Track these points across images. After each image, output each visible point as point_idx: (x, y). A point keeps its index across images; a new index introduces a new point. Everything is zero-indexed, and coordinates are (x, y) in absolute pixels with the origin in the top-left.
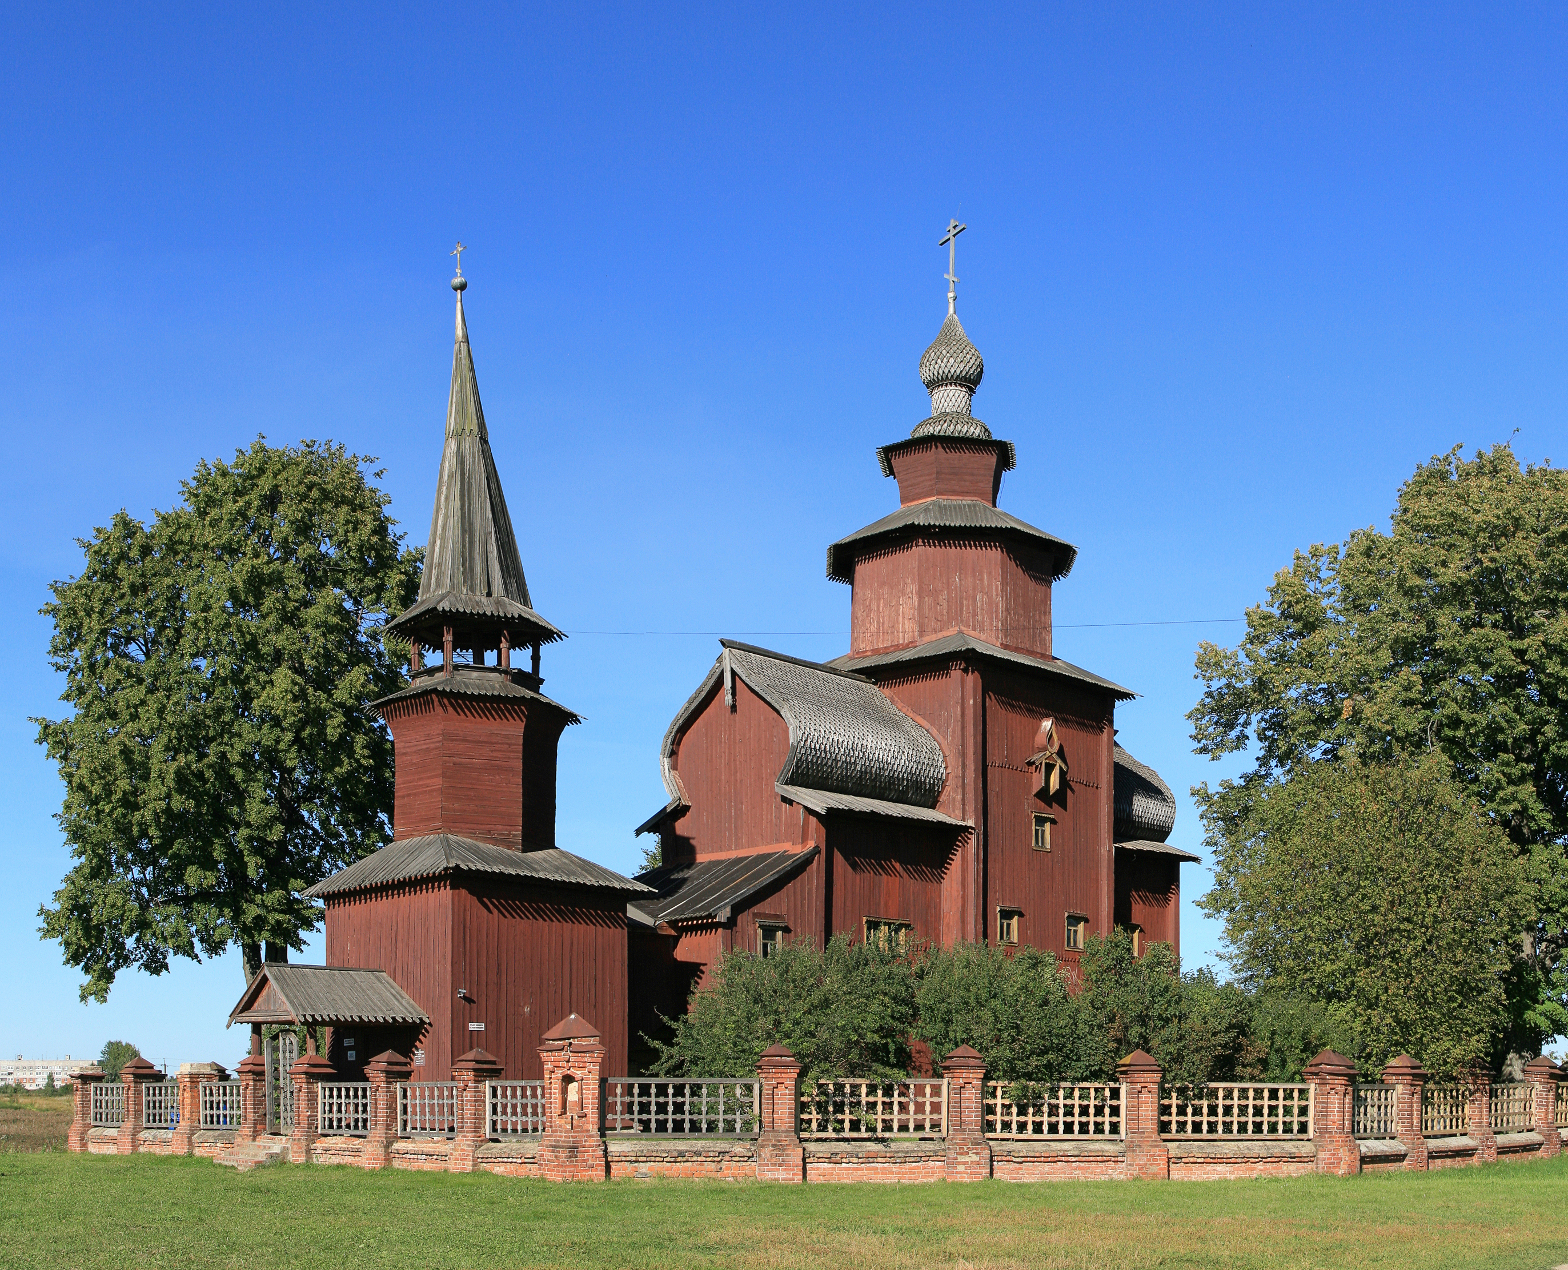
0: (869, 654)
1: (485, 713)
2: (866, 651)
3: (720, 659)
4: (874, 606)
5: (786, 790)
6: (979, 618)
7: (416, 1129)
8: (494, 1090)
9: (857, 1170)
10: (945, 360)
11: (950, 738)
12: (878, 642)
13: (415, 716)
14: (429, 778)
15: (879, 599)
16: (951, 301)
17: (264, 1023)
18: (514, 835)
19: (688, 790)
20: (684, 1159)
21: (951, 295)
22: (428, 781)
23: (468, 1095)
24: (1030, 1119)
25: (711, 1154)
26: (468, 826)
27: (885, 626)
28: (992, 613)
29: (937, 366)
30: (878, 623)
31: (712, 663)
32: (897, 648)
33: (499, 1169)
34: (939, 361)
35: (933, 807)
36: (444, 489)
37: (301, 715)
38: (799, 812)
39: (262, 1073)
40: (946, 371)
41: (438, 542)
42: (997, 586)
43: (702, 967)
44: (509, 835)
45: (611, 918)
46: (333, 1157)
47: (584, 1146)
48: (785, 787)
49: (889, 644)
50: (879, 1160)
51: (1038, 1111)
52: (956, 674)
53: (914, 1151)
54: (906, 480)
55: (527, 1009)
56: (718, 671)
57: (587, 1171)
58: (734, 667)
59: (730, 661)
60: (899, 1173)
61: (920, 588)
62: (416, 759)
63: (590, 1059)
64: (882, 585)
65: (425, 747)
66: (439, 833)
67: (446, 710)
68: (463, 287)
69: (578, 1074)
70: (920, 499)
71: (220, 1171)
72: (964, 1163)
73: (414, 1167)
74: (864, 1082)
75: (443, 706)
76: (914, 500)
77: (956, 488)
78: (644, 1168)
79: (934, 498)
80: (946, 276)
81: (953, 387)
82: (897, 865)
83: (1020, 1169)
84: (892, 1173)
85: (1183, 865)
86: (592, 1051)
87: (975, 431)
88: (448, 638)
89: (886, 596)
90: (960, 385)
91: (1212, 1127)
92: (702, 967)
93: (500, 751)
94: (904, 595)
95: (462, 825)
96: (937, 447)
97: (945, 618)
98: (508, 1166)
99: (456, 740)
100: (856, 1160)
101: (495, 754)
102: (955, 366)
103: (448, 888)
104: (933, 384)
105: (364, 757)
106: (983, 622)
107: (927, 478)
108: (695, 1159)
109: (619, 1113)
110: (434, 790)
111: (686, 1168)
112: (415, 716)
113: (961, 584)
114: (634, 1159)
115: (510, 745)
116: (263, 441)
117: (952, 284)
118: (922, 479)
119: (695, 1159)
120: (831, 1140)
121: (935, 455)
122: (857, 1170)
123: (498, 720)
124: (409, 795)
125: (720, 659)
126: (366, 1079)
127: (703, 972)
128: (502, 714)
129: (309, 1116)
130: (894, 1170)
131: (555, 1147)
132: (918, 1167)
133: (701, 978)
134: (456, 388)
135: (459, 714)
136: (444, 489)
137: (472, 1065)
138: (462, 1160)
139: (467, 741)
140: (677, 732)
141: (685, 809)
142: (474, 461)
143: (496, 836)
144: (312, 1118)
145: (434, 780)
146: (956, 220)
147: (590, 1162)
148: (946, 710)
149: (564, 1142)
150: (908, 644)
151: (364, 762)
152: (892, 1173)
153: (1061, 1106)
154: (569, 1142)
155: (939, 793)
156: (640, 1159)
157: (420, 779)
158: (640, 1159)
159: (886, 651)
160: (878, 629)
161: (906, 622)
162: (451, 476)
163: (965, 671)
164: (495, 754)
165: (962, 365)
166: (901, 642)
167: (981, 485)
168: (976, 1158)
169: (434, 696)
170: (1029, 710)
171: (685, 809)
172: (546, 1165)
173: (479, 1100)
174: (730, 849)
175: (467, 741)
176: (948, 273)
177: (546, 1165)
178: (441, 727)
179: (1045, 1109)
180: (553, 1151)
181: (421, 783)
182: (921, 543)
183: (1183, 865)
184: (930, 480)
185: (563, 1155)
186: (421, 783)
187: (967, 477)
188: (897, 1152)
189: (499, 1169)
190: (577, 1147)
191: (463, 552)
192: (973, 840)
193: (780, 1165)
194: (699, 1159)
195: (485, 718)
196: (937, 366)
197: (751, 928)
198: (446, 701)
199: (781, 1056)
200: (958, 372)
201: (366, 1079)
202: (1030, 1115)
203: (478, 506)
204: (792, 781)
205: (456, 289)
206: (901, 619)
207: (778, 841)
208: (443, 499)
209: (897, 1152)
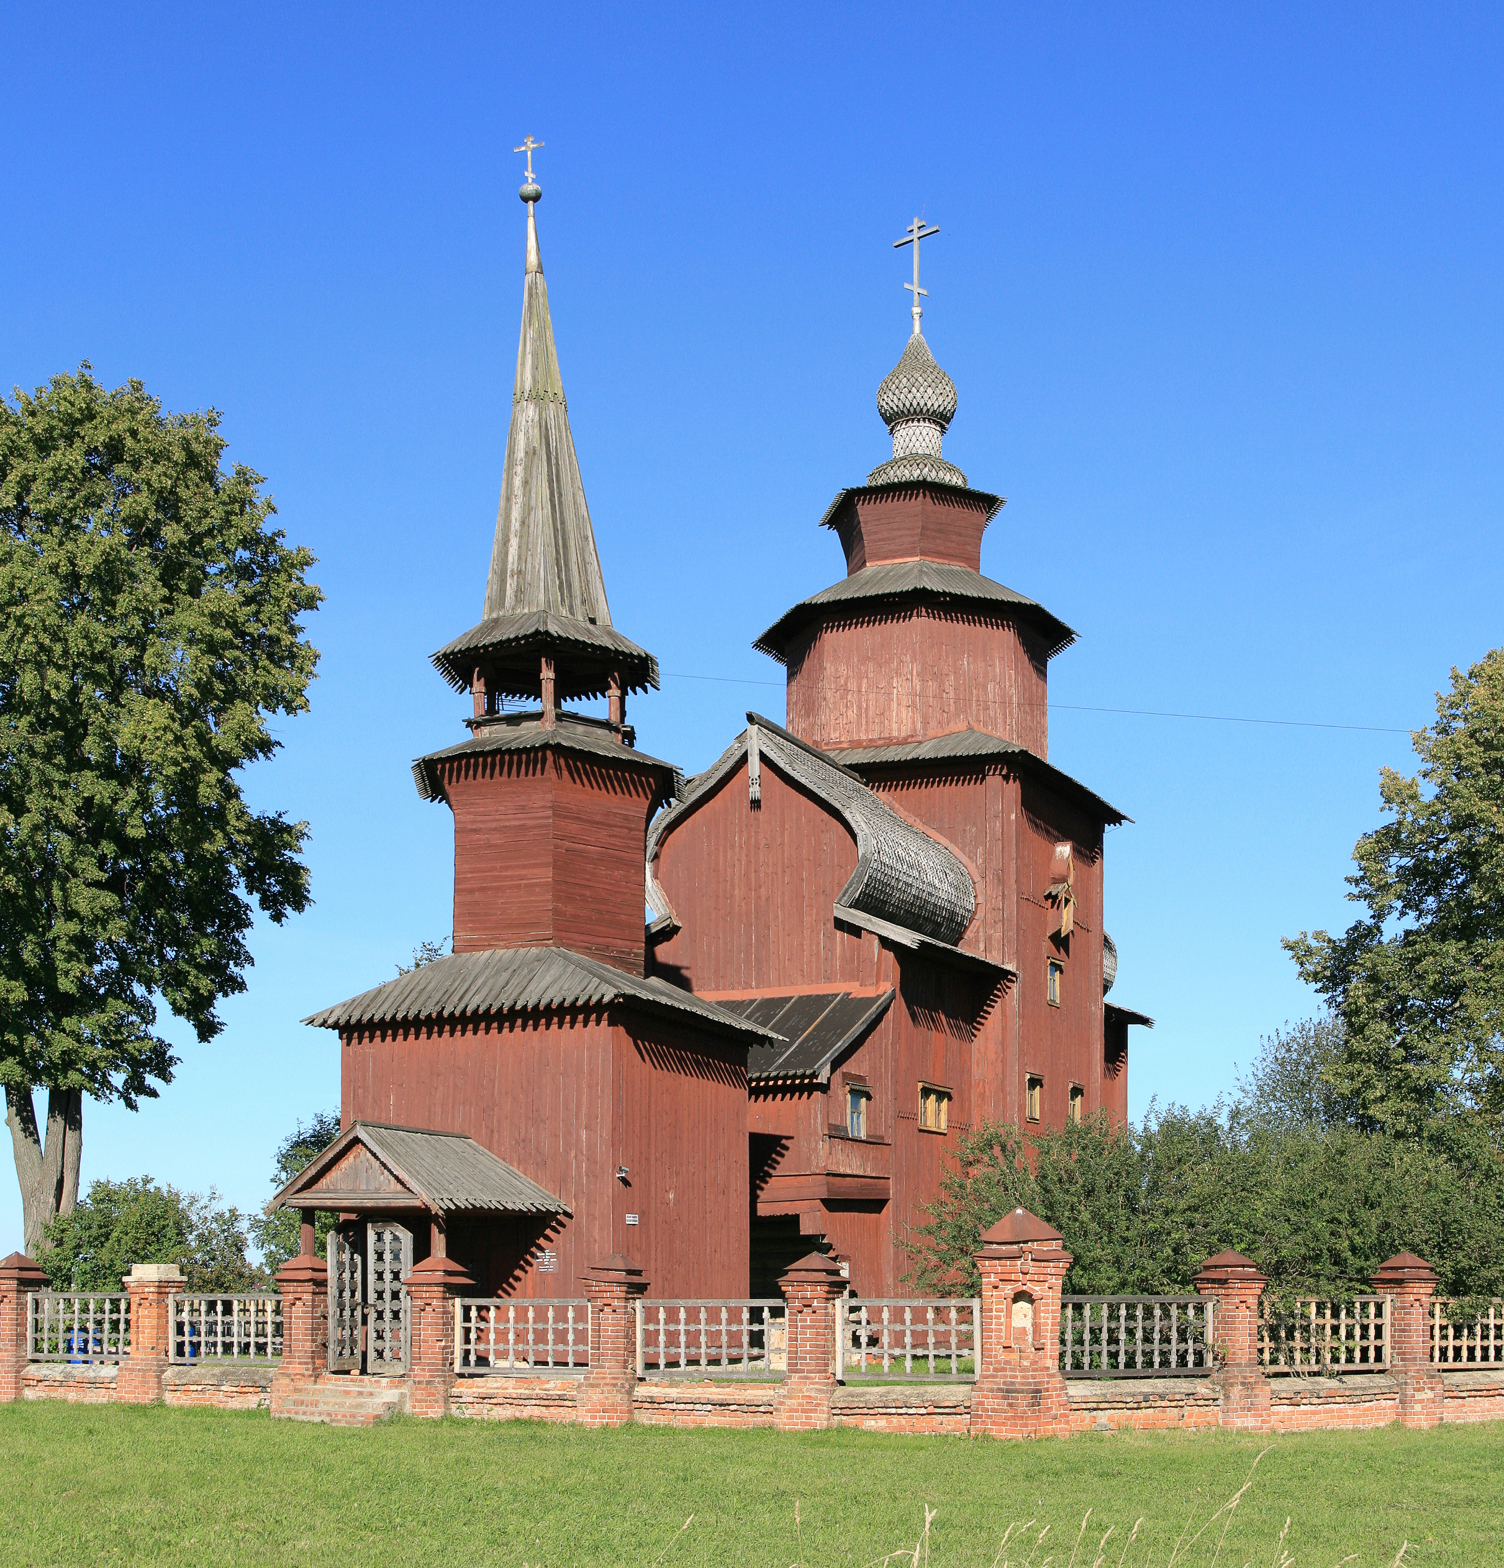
0: (845, 745)
1: (606, 783)
2: (841, 742)
3: (741, 737)
4: (852, 685)
5: (852, 914)
6: (992, 714)
7: (655, 1366)
8: (467, 1309)
9: (1314, 1413)
10: (922, 389)
11: (980, 861)
12: (859, 731)
13: (504, 778)
14: (524, 867)
15: (860, 678)
16: (916, 317)
17: (321, 1208)
18: (636, 955)
19: (677, 906)
20: (1148, 1404)
21: (916, 310)
22: (524, 872)
23: (429, 1316)
24: (1464, 1342)
25: (1178, 1397)
26: (582, 937)
27: (871, 713)
28: (1005, 708)
29: (910, 396)
30: (859, 707)
31: (730, 742)
32: (889, 742)
33: (870, 1424)
34: (914, 390)
35: (922, 942)
36: (519, 469)
37: (186, 765)
38: (871, 945)
39: (323, 1283)
40: (922, 404)
41: (514, 542)
42: (1010, 675)
43: (784, 1142)
44: (629, 954)
45: (736, 1073)
46: (496, 1408)
47: (1047, 1390)
48: (852, 910)
49: (876, 736)
50: (1338, 1399)
51: (1472, 1334)
52: (994, 781)
53: (1371, 1388)
54: (876, 533)
55: (671, 1196)
56: (738, 754)
57: (1050, 1423)
58: (765, 750)
59: (757, 741)
60: (1353, 1416)
61: (924, 668)
62: (497, 839)
63: (1053, 1271)
64: (864, 660)
65: (517, 823)
66: (547, 946)
67: (560, 776)
68: (536, 198)
69: (1036, 1290)
70: (895, 557)
71: (683, 1438)
72: (1421, 1401)
73: (689, 1421)
74: (1313, 1300)
75: (558, 768)
76: (886, 558)
77: (942, 549)
78: (1103, 1417)
79: (917, 559)
80: (907, 286)
81: (922, 423)
82: (943, 1017)
83: (1464, 1405)
84: (1347, 1416)
85: (1133, 1030)
86: (1058, 1260)
87: (956, 481)
88: (547, 674)
89: (871, 675)
90: (934, 421)
91: (196, 1346)
92: (784, 1142)
93: (619, 837)
94: (898, 674)
95: (576, 936)
96: (925, 496)
97: (952, 708)
98: (895, 1419)
99: (565, 817)
100: (1316, 1401)
101: (612, 840)
102: (933, 399)
103: (604, 1023)
104: (892, 419)
105: (239, 831)
106: (996, 719)
107: (907, 532)
108: (1159, 1403)
109: (551, 1342)
110: (536, 885)
111: (1147, 1416)
112: (504, 778)
113: (969, 670)
114: (1094, 1405)
115: (631, 829)
116: (86, 372)
117: (916, 297)
118: (899, 533)
119: (1159, 1403)
120: (1371, 1372)
121: (919, 504)
122: (1314, 1413)
123: (620, 794)
124: (482, 889)
125: (741, 737)
126: (781, 1295)
127: (786, 1148)
128: (624, 786)
129: (445, 1347)
130: (1350, 1412)
131: (1008, 1391)
132: (1371, 1408)
133: (782, 1156)
134: (531, 333)
135: (575, 782)
136: (519, 469)
137: (823, 1276)
138: (804, 1411)
139: (580, 819)
140: (665, 829)
141: (676, 929)
142: (560, 437)
143: (614, 954)
144: (448, 1350)
145: (536, 871)
146: (921, 220)
147: (1054, 1412)
148: (975, 824)
149: (1020, 1384)
150: (906, 739)
151: (236, 837)
152: (1347, 1416)
153: (1492, 1326)
154: (1029, 1384)
155: (966, 928)
156: (1102, 1406)
157: (507, 868)
158: (1102, 1406)
159: (871, 744)
160: (859, 716)
161: (904, 710)
162: (531, 453)
163: (1006, 778)
164: (612, 840)
165: (941, 399)
166: (895, 734)
167: (969, 548)
168: (1430, 1394)
169: (549, 753)
170: (1048, 832)
171: (676, 929)
172: (990, 1417)
173: (448, 1323)
174: (748, 986)
175: (580, 819)
176: (912, 283)
177: (990, 1417)
178: (550, 797)
179: (1478, 1330)
180: (1004, 1398)
181: (509, 873)
182: (924, 613)
183: (1133, 1030)
184: (912, 536)
185: (1022, 1402)
186: (509, 873)
187: (954, 537)
188: (1356, 1389)
189: (870, 1424)
190: (1039, 1391)
191: (557, 560)
192: (1015, 988)
193: (1249, 1410)
194: (1163, 1404)
195: (604, 791)
196: (910, 396)
197: (840, 1093)
198: (562, 761)
199: (1243, 1266)
200: (936, 407)
201: (781, 1295)
202: (1464, 1339)
203: (570, 497)
204: (857, 905)
205: (526, 199)
206: (894, 705)
207: (829, 979)
208: (517, 482)
209: (1356, 1389)
